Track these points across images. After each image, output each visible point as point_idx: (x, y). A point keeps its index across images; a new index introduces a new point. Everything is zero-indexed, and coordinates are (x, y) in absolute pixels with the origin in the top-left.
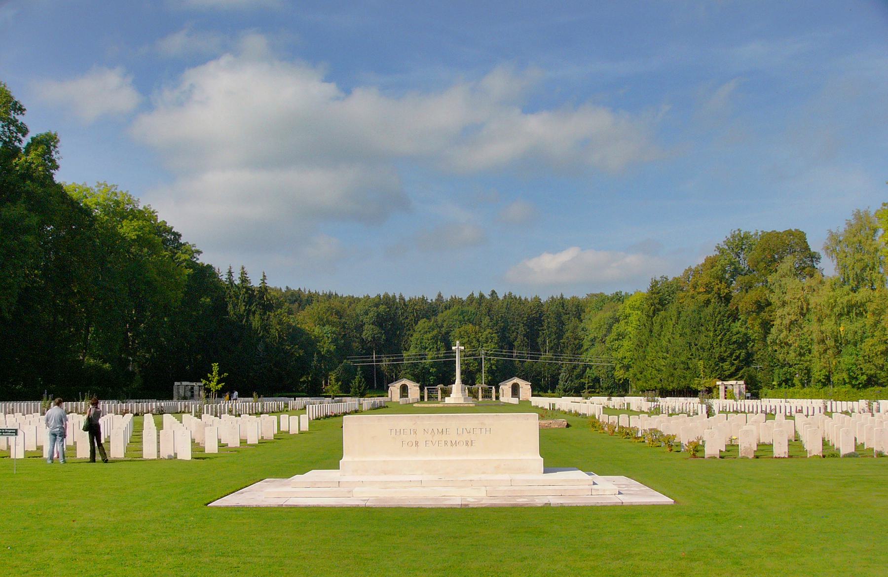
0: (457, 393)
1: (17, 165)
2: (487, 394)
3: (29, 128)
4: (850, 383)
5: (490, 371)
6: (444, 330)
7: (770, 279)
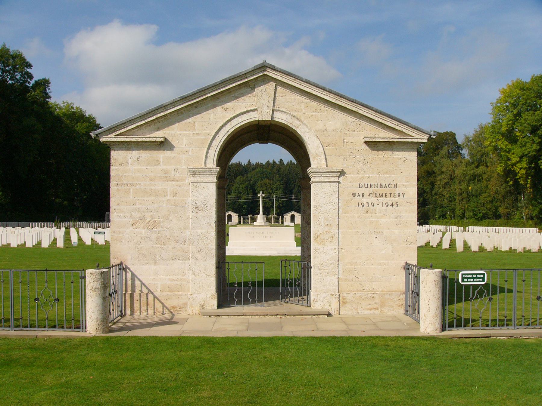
0: (260, 218)
1: (29, 97)
2: (277, 220)
3: (33, 75)
4: (474, 217)
5: (278, 207)
6: (251, 183)
7: (435, 159)
